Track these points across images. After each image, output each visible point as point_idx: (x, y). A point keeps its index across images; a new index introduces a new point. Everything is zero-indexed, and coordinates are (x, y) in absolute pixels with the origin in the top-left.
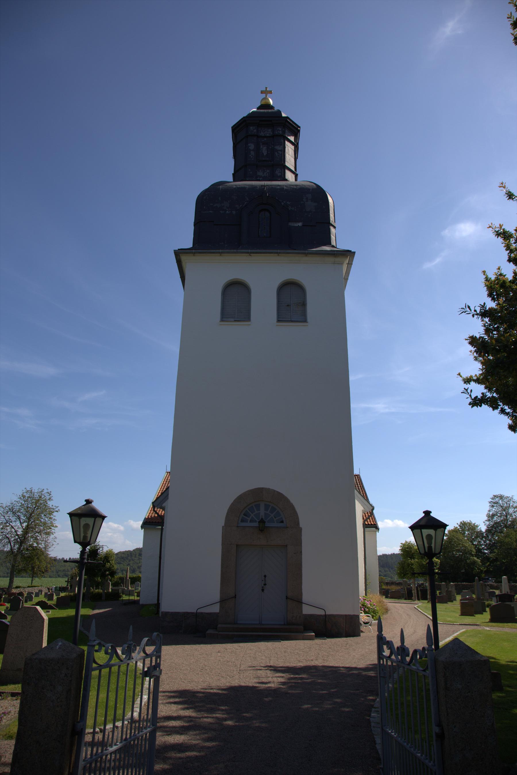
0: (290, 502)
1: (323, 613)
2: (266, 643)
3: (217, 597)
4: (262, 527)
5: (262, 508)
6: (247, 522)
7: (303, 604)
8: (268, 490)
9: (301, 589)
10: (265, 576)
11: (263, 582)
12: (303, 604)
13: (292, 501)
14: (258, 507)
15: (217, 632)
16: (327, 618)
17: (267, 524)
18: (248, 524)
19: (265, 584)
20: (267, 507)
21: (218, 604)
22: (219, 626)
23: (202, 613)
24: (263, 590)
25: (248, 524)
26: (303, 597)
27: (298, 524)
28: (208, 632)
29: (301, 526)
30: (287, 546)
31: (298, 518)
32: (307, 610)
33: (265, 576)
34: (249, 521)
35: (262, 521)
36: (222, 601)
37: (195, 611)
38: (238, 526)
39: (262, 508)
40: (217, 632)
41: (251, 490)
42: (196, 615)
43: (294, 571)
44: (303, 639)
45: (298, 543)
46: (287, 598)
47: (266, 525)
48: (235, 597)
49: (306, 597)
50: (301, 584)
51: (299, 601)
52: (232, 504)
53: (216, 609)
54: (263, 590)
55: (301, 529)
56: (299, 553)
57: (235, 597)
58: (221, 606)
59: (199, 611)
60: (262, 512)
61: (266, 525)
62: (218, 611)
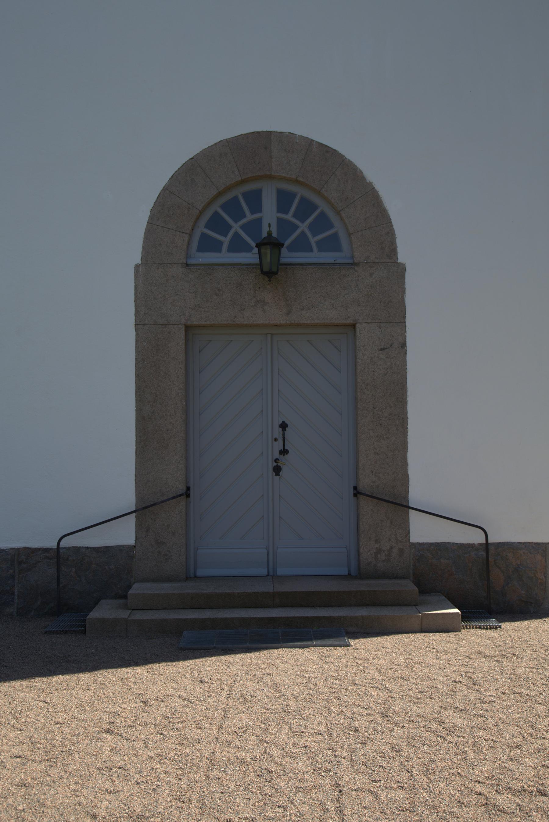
0: (363, 178)
1: (477, 538)
2: (297, 652)
3: (126, 496)
4: (272, 264)
5: (269, 203)
6: (220, 251)
7: (412, 513)
8: (286, 140)
9: (405, 464)
10: (284, 426)
11: (279, 446)
12: (413, 514)
13: (371, 175)
14: (255, 200)
15: (124, 614)
16: (489, 556)
17: (287, 256)
18: (225, 257)
19: (284, 452)
20: (284, 200)
21: (132, 520)
22: (137, 589)
23: (77, 549)
24: (277, 470)
25: (225, 257)
26: (411, 489)
27: (393, 252)
28: (94, 614)
29: (402, 258)
30: (354, 326)
31: (390, 233)
32: (423, 531)
33: (284, 426)
34: (225, 247)
35: (272, 244)
36: (144, 509)
37: (53, 544)
38: (187, 265)
39: (269, 203)
40: (124, 614)
41: (227, 141)
42: (57, 556)
43: (380, 407)
44: (422, 631)
45: (394, 313)
46: (357, 492)
47: (283, 260)
48: (188, 496)
49: (418, 492)
50: (403, 446)
51: (397, 503)
52: (165, 189)
53: (124, 534)
54: (277, 470)
55: (401, 270)
56: (396, 348)
57: (187, 493)
58: (139, 526)
59: (65, 543)
60: (269, 215)
61: (283, 260)
62: (130, 540)
